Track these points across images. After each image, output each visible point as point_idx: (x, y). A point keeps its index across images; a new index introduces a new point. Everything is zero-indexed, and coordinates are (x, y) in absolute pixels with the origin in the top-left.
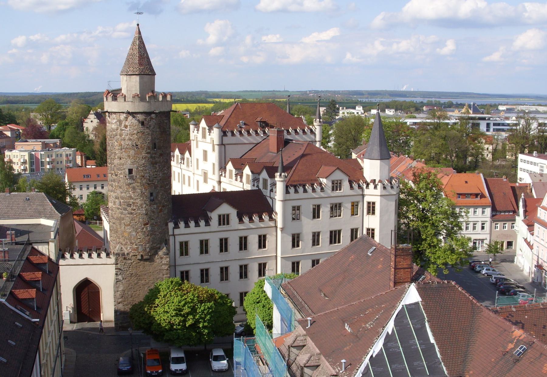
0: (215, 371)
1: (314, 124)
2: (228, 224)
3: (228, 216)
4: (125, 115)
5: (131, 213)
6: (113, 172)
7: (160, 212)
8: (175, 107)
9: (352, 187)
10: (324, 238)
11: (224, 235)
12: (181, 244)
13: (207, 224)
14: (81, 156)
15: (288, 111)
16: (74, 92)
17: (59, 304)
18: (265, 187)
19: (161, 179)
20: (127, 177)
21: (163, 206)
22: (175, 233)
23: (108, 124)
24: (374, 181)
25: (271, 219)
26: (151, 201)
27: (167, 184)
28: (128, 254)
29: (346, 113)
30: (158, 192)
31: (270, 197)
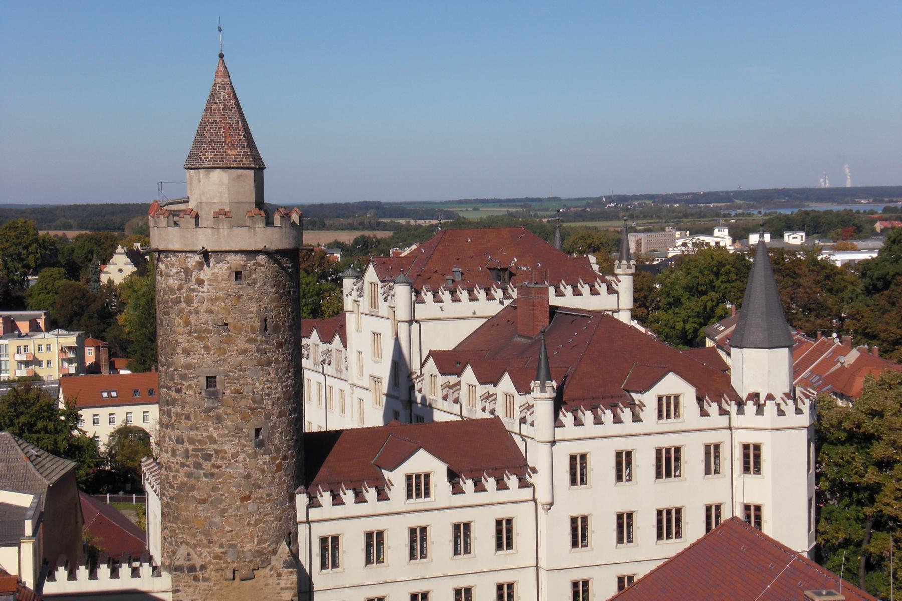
0: (420, 448)
1: (617, 271)
2: (428, 494)
4: (198, 258)
5: (212, 475)
6: (171, 384)
7: (277, 471)
8: (311, 238)
9: (704, 414)
10: (645, 526)
11: (417, 521)
12: (324, 540)
13: (382, 496)
14: (97, 348)
15: (558, 247)
16: (786, 545)
18: (509, 413)
20: (203, 394)
22: (310, 519)
23: (159, 278)
24: (755, 397)
25: (523, 484)
28: (203, 568)
29: (690, 245)
30: (274, 427)
31: (521, 436)
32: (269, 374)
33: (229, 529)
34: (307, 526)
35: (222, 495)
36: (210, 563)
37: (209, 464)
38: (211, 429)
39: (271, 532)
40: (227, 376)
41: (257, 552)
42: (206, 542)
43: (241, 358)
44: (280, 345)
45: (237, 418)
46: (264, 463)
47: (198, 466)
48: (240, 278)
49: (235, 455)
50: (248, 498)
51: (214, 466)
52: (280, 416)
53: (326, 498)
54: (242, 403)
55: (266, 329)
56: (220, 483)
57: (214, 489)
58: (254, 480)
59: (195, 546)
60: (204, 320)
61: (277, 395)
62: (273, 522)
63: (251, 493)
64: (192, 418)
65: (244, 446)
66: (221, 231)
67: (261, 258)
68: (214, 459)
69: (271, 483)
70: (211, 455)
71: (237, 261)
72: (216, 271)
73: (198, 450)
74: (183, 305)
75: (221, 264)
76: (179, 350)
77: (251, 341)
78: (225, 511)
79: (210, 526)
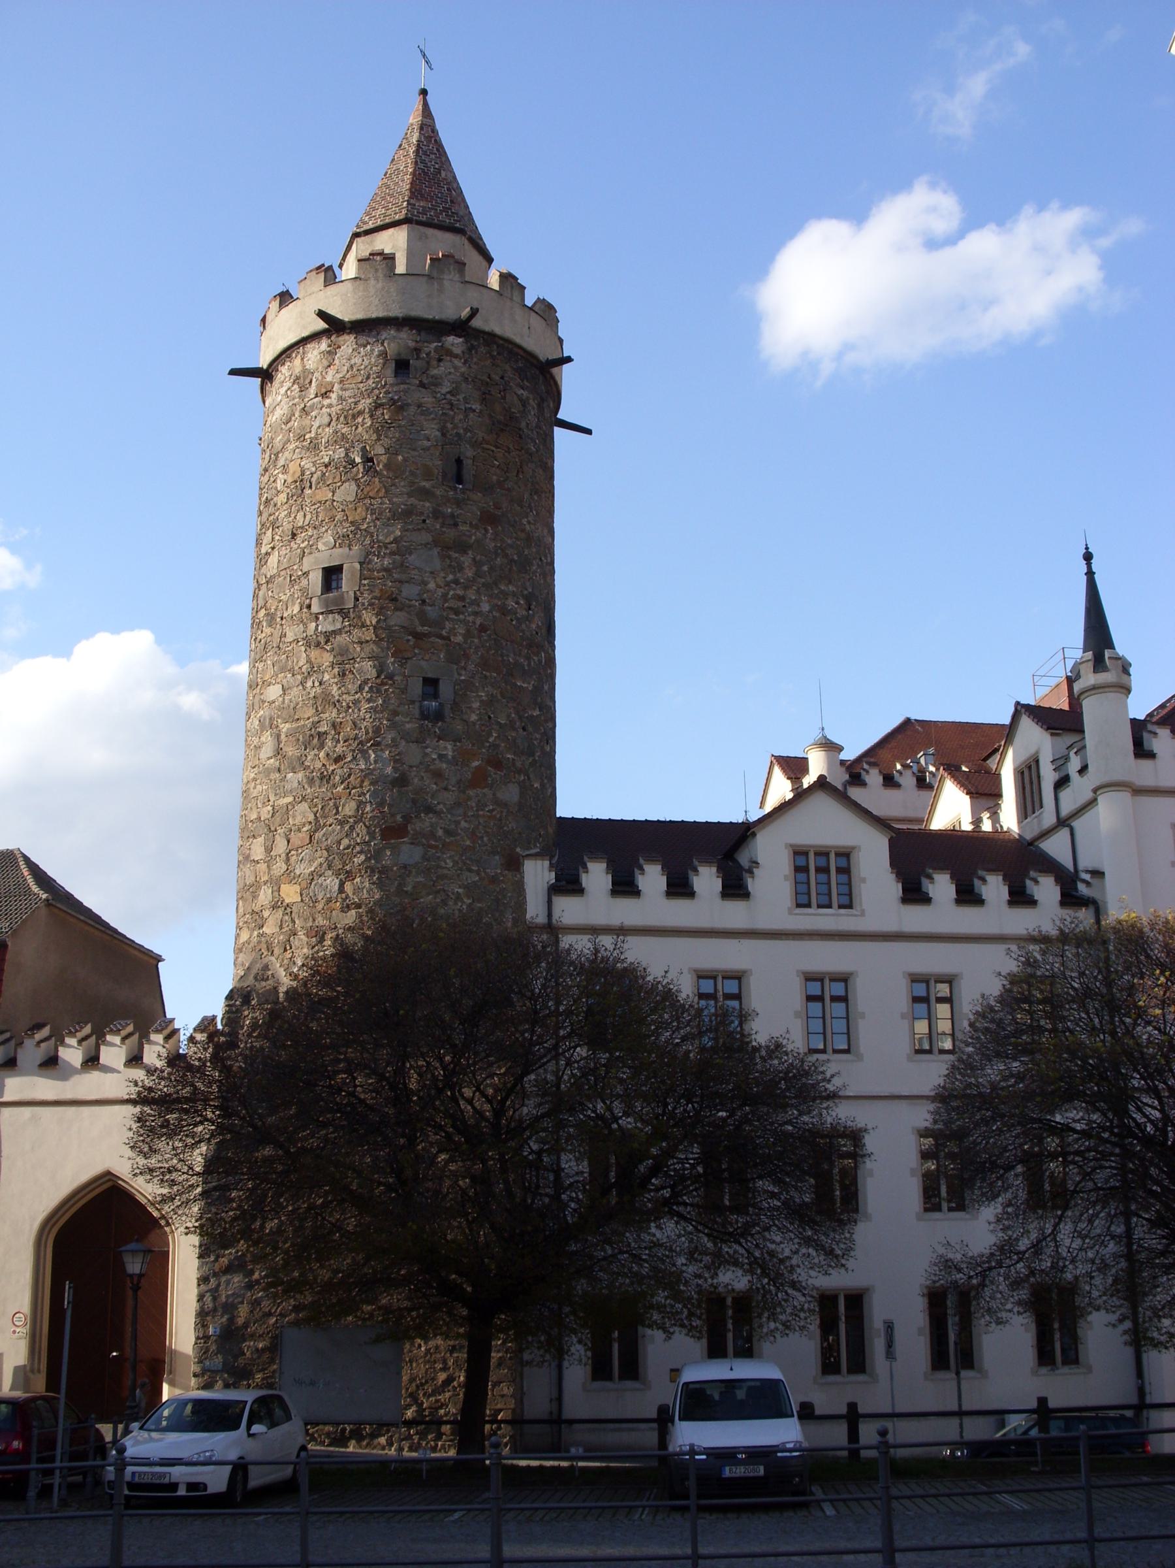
3: (845, 854)
17: (186, 1474)
19: (483, 628)
21: (498, 764)
26: (424, 715)
27: (546, 721)
46: (441, 757)
63: (407, 819)
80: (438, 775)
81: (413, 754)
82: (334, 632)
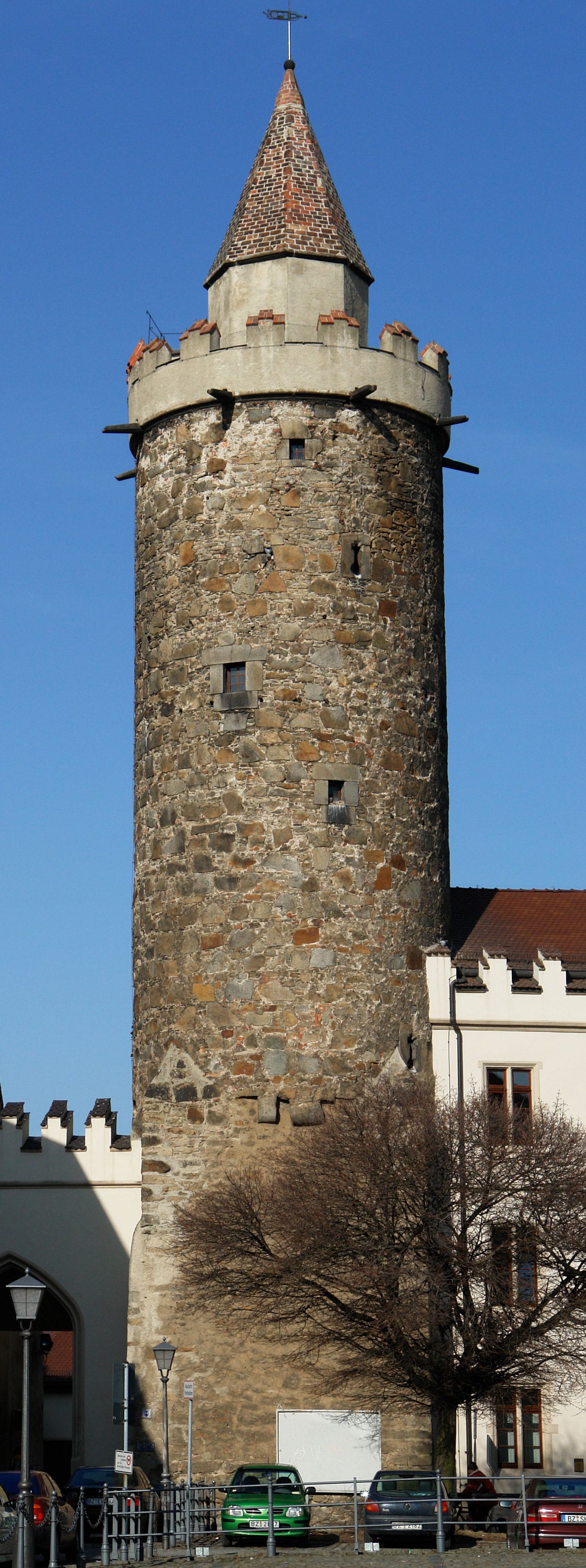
4: (213, 417)
5: (233, 881)
20: (217, 706)
28: (210, 1092)
30: (371, 786)
32: (363, 666)
33: (266, 1001)
34: (453, 1034)
35: (252, 925)
36: (226, 1077)
37: (227, 856)
38: (232, 779)
39: (366, 1021)
40: (267, 661)
41: (333, 1060)
42: (217, 1032)
43: (296, 624)
44: (387, 609)
45: (288, 753)
46: (349, 861)
47: (203, 864)
48: (301, 456)
49: (282, 838)
50: (310, 935)
51: (237, 861)
52: (387, 763)
53: (496, 972)
54: (302, 720)
55: (356, 569)
56: (250, 898)
57: (237, 912)
58: (326, 896)
59: (196, 1045)
60: (221, 547)
61: (380, 718)
62: (368, 1000)
63: (318, 923)
64: (194, 762)
65: (303, 817)
66: (263, 350)
67: (349, 416)
68: (236, 846)
69: (365, 907)
70: (231, 837)
71: (292, 417)
72: (249, 438)
73: (204, 829)
74: (182, 523)
75: (261, 424)
76: (172, 621)
77: (325, 587)
78: (260, 960)
79: (227, 996)
80: (346, 879)
81: (320, 857)
82: (238, 732)
